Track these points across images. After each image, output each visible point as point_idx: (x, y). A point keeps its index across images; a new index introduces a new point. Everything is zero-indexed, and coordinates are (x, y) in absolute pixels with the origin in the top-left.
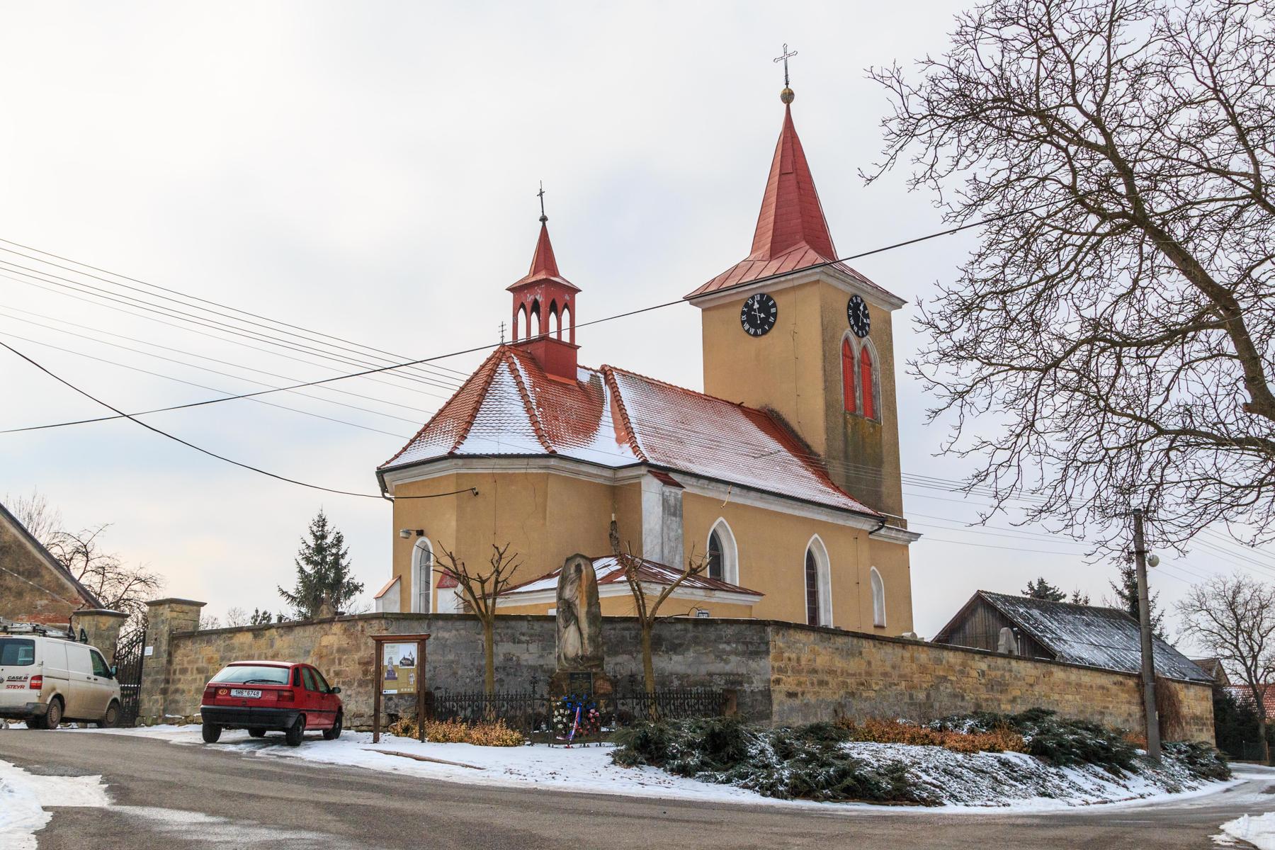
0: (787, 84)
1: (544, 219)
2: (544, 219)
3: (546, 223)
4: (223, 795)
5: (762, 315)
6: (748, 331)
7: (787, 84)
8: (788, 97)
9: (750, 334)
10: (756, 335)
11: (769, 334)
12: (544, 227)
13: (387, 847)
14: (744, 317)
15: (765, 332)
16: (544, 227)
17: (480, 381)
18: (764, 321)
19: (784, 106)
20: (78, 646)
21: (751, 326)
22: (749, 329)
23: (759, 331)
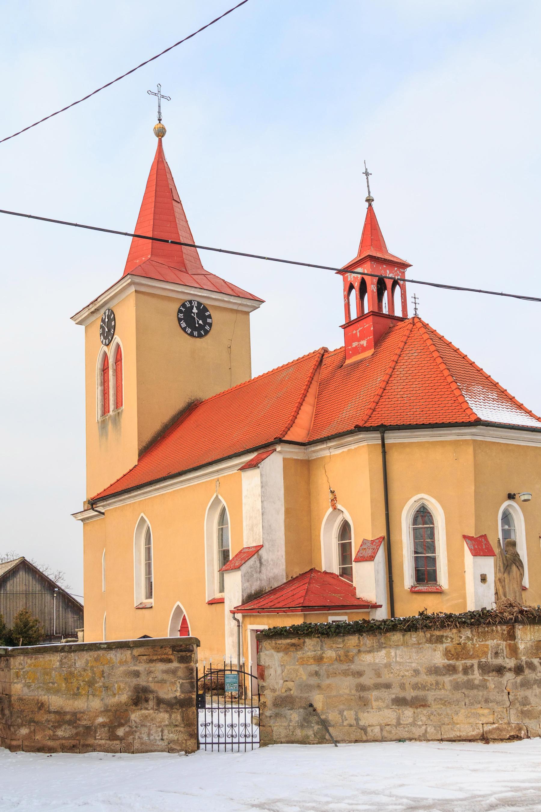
0: (160, 120)
1: (369, 200)
2: (369, 200)
3: (373, 203)
4: (424, 687)
5: (201, 322)
6: (184, 329)
7: (160, 120)
8: (161, 133)
9: (186, 333)
10: (191, 335)
11: (194, 339)
12: (370, 209)
13: (453, 614)
14: (181, 316)
15: (200, 336)
16: (370, 209)
17: (259, 300)
18: (201, 327)
19: (157, 139)
20: (297, 746)
21: (188, 325)
22: (185, 328)
23: (196, 333)
